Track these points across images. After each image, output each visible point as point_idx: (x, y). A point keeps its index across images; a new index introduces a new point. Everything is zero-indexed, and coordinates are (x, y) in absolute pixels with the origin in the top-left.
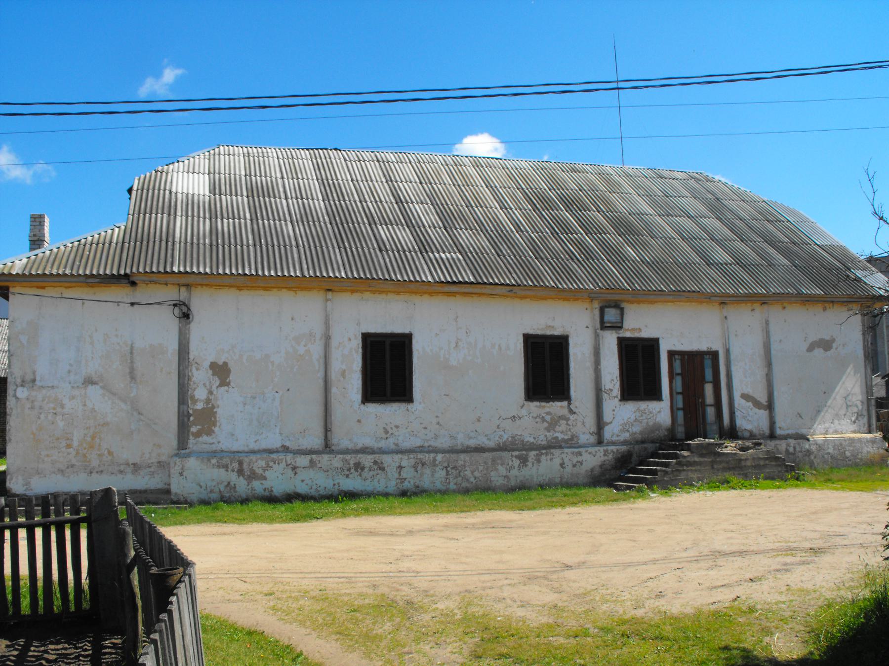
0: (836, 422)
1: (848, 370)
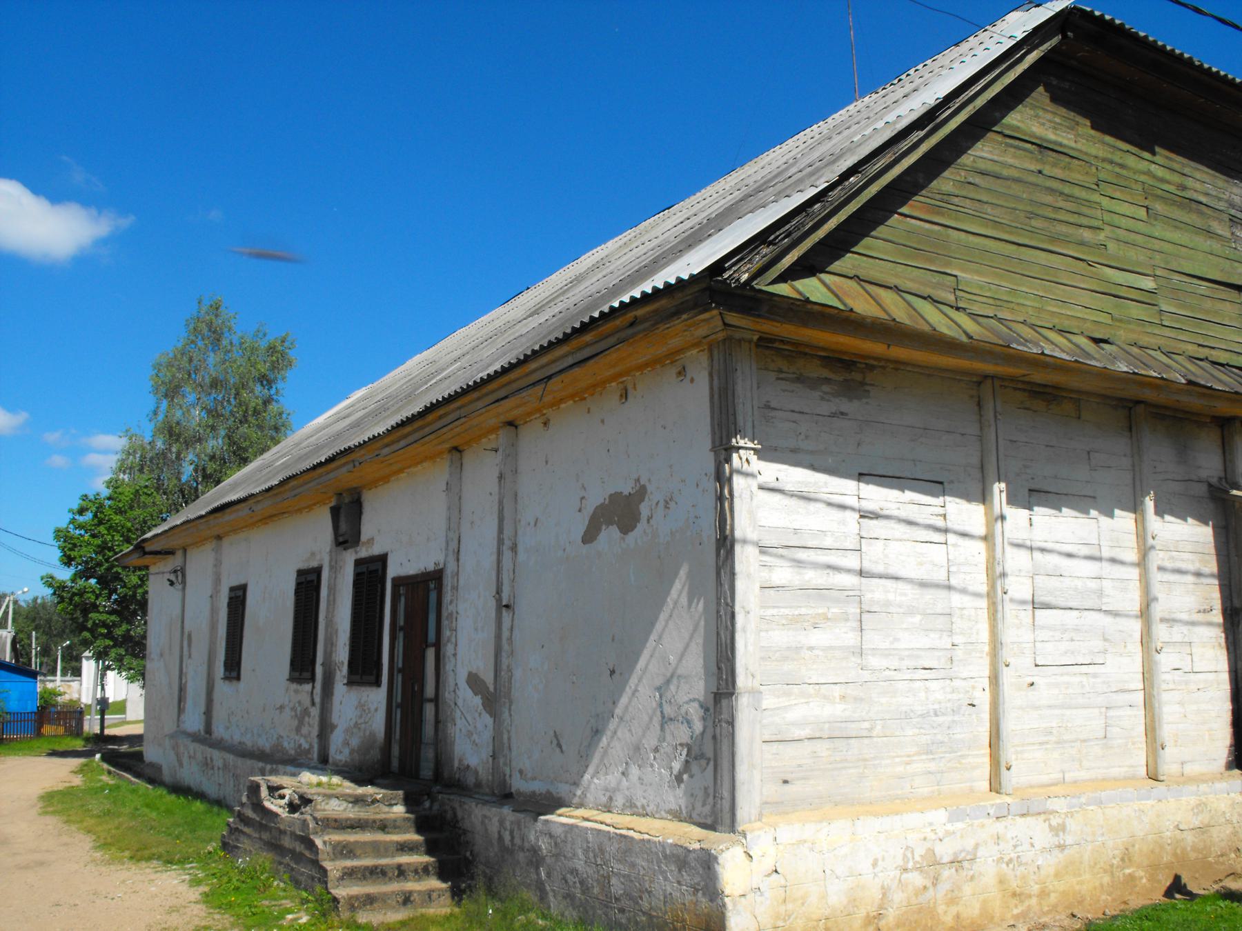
0: (634, 771)
1: (674, 593)
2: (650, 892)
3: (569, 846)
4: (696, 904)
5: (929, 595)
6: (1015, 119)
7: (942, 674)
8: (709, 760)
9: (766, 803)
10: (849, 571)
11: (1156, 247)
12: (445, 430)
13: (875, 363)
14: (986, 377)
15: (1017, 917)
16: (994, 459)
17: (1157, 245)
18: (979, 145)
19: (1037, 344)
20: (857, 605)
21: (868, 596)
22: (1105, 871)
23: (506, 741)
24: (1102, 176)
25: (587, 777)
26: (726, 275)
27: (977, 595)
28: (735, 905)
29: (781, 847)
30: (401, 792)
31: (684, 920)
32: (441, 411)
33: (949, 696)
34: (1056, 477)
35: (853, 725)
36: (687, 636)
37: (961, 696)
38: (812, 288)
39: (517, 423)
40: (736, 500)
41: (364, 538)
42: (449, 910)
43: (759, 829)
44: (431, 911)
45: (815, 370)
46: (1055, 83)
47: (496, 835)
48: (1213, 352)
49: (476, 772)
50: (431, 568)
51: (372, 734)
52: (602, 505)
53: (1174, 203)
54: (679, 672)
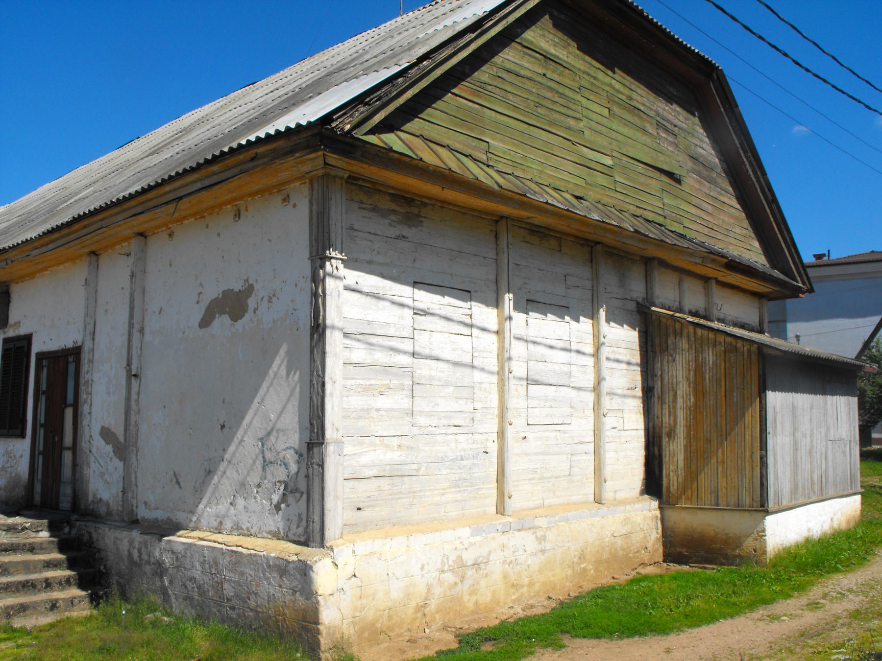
0: (241, 502)
1: (275, 366)
2: (256, 594)
3: (188, 560)
4: (294, 602)
5: (460, 371)
6: (530, 35)
7: (466, 430)
8: (302, 493)
9: (345, 525)
10: (405, 353)
11: (614, 137)
12: (88, 237)
13: (428, 201)
14: (502, 217)
15: (514, 601)
16: (506, 276)
17: (614, 135)
18: (506, 50)
19: (543, 197)
20: (410, 379)
21: (418, 372)
22: (569, 567)
23: (133, 479)
24: (583, 83)
25: (201, 506)
26: (334, 125)
27: (491, 373)
28: (325, 602)
29: (358, 558)
30: (45, 521)
31: (284, 614)
32: (86, 222)
33: (471, 446)
34: (544, 292)
35: (406, 467)
36: (284, 399)
37: (479, 446)
38: (391, 140)
39: (97, 253)
40: (328, 298)
41: (11, 321)
42: (89, 613)
43: (343, 544)
44: (75, 614)
45: (386, 204)
46: (556, 14)
47: (126, 553)
48: (645, 212)
49: (108, 504)
50: (70, 345)
51: (18, 476)
52: (216, 299)
53: (625, 108)
54: (278, 426)
